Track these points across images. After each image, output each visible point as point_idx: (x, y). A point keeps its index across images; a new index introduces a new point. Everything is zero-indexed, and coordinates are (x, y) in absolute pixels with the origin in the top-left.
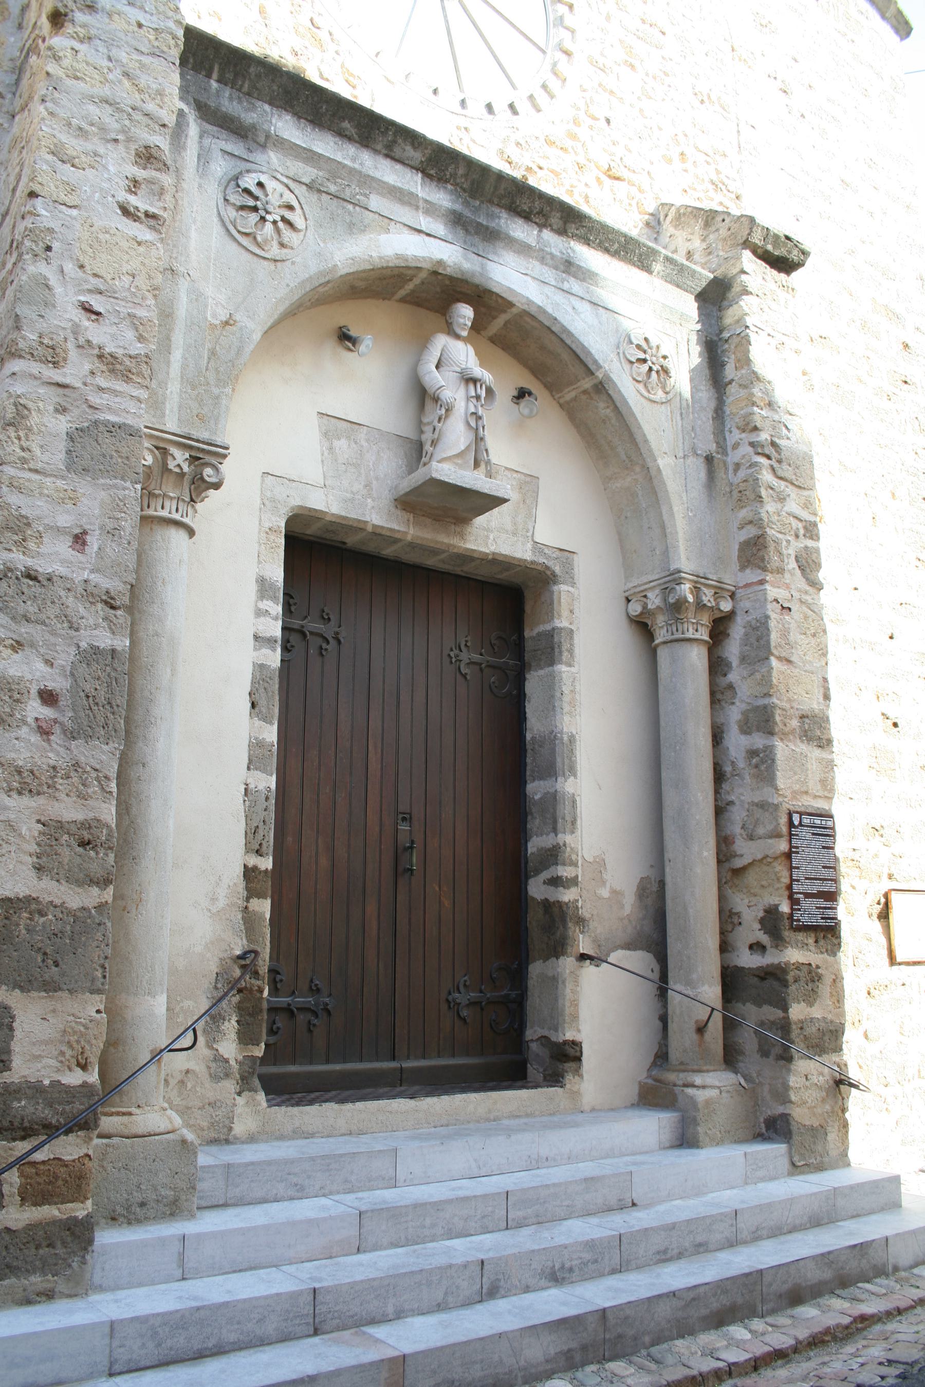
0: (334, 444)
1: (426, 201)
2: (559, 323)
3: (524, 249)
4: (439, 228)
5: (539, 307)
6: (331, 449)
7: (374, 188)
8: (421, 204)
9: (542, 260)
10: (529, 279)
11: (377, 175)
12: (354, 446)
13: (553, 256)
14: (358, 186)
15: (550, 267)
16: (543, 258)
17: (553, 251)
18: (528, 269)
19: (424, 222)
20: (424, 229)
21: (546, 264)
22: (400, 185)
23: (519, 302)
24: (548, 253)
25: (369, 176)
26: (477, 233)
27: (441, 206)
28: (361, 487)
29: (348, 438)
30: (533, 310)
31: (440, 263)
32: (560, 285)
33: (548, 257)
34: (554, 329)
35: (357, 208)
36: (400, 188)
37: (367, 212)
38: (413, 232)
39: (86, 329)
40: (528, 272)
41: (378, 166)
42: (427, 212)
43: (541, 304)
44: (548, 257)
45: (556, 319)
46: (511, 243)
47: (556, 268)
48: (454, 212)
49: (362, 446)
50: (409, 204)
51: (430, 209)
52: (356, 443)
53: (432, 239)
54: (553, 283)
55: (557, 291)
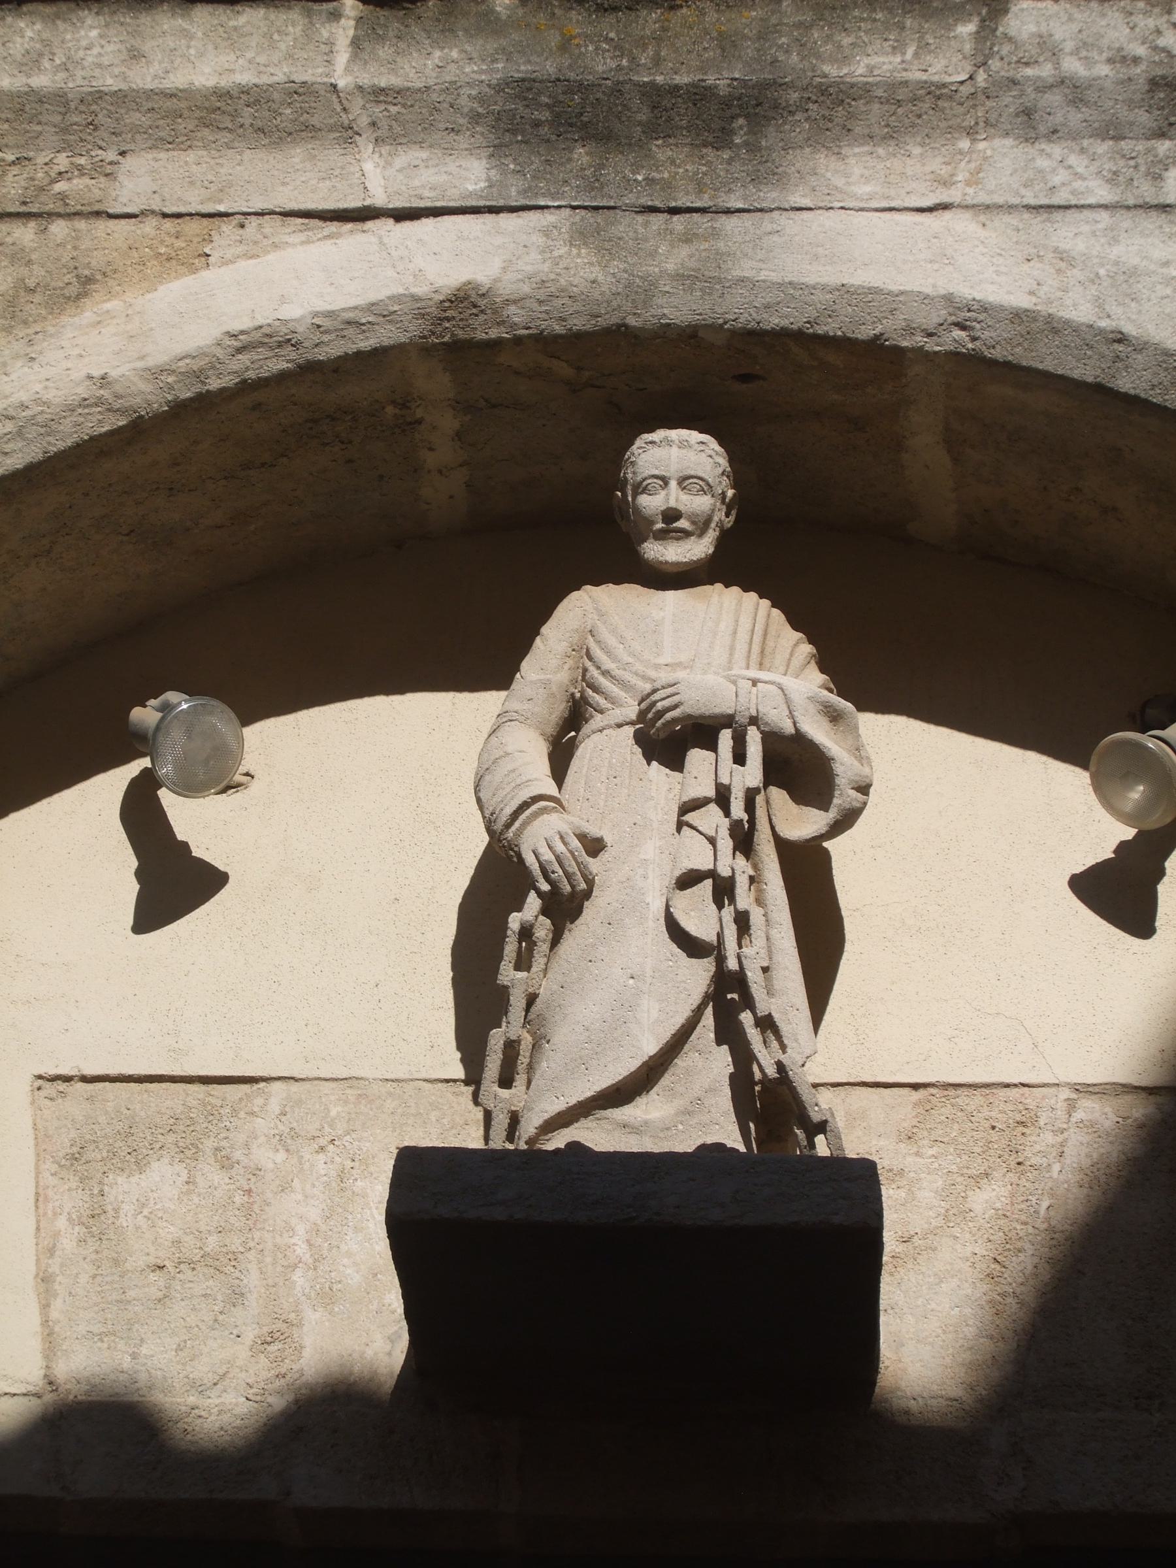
0: (112, 1194)
1: (378, 94)
2: (1141, 347)
3: (916, 111)
4: (470, 173)
5: (1018, 315)
6: (96, 1220)
7: (136, 130)
8: (361, 115)
9: (1029, 124)
10: (959, 223)
11: (144, 78)
12: (218, 1177)
13: (1076, 92)
14: (66, 147)
15: (1074, 136)
16: (1027, 113)
17: (1072, 66)
18: (947, 183)
19: (378, 176)
20: (379, 198)
21: (1053, 133)
22: (245, 78)
23: (910, 330)
24: (1044, 88)
25: (99, 95)
26: (653, 130)
27: (452, 88)
28: (242, 1352)
29: (188, 1152)
30: (997, 343)
31: (464, 300)
32: (1146, 191)
33: (1054, 98)
34: (1124, 384)
35: (59, 228)
36: (245, 91)
37: (102, 225)
38: (333, 227)
39: (871, 69)
40: (952, 195)
41: (147, 47)
42: (390, 137)
43: (1022, 301)
44: (1054, 98)
45: (1121, 338)
46: (837, 111)
47: (1112, 131)
48: (523, 89)
49: (256, 1172)
50: (305, 131)
51: (403, 117)
52: (226, 1163)
53: (427, 225)
54: (1102, 193)
55: (1125, 220)
